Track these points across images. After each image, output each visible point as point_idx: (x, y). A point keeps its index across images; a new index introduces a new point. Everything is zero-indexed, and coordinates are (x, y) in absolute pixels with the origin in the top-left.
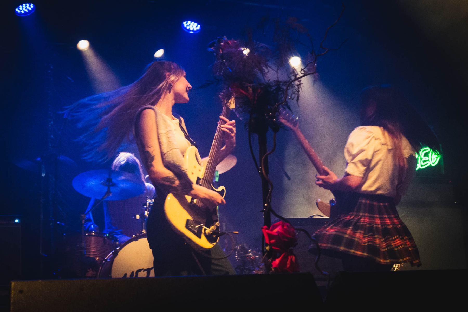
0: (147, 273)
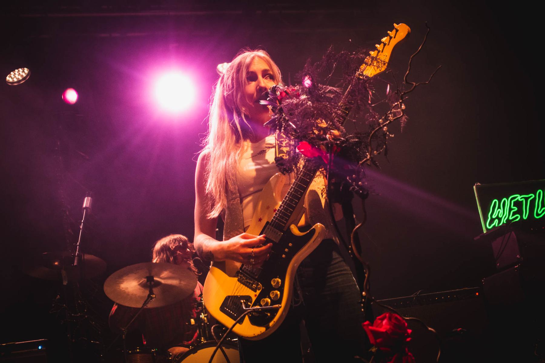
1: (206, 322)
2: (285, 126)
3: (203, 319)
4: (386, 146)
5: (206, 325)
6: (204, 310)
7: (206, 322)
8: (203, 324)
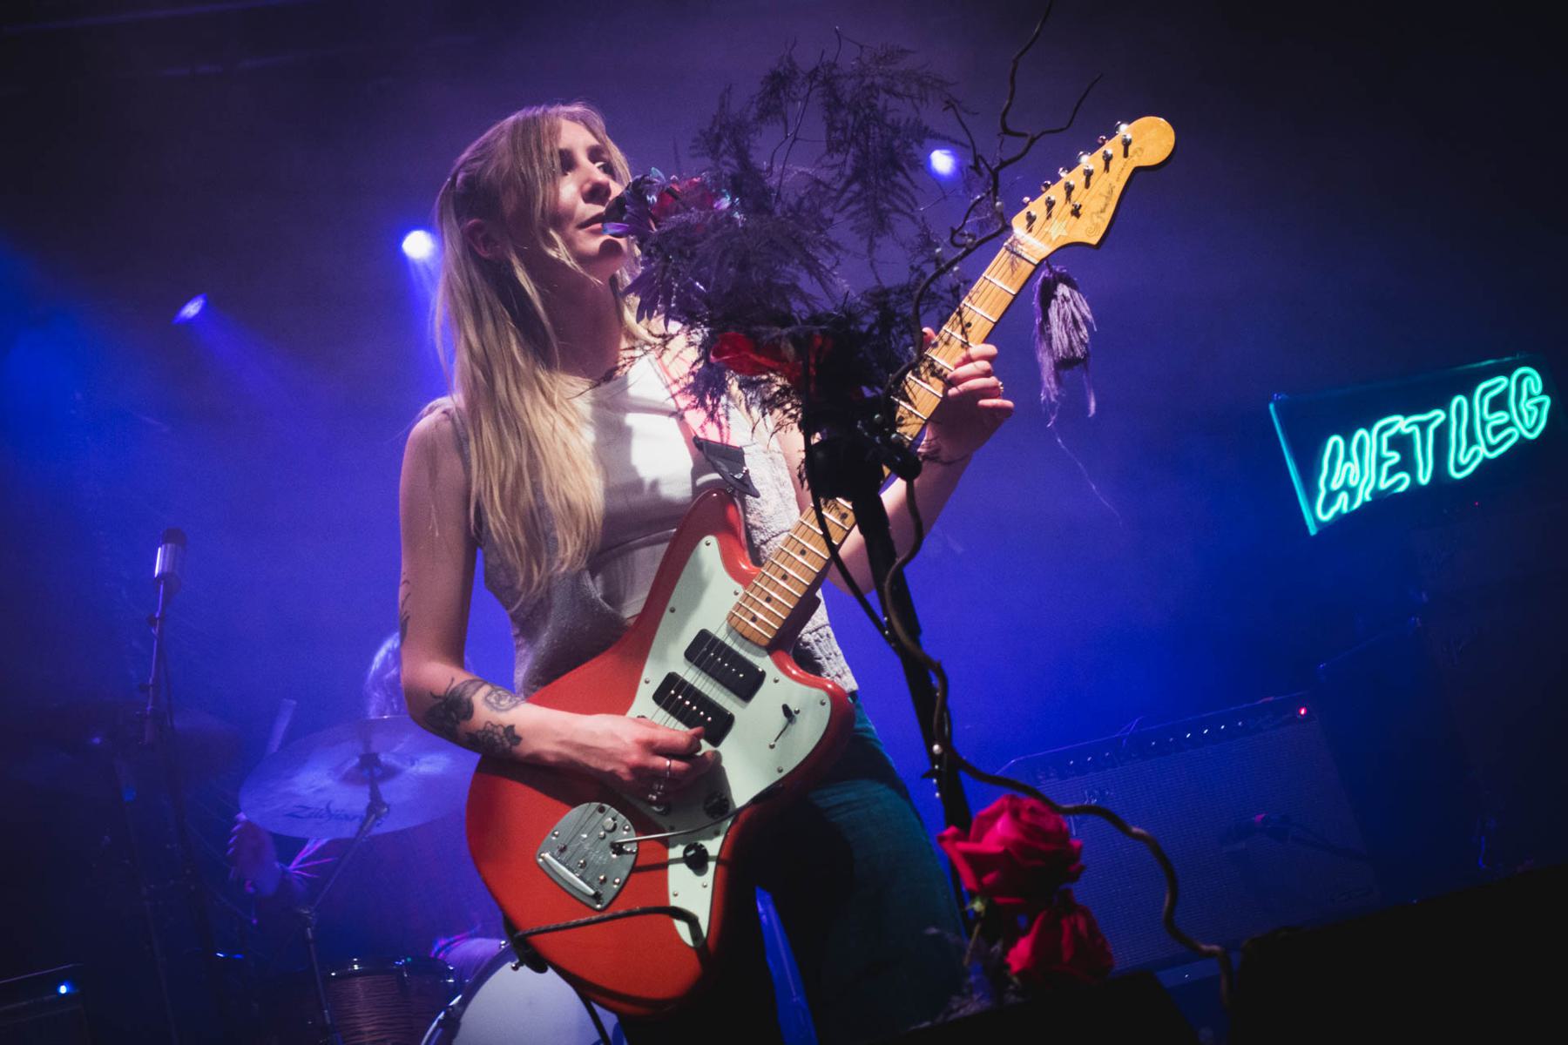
0: (678, 918)
2: (678, 289)
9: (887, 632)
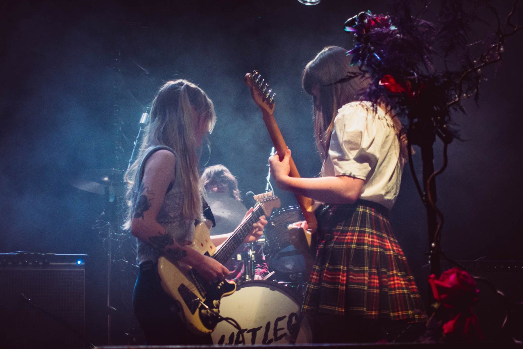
0: (277, 328)
1: (253, 259)
2: (369, 56)
3: (251, 256)
4: (478, 90)
5: (253, 262)
6: (252, 247)
7: (253, 259)
8: (249, 261)
9: (424, 198)
